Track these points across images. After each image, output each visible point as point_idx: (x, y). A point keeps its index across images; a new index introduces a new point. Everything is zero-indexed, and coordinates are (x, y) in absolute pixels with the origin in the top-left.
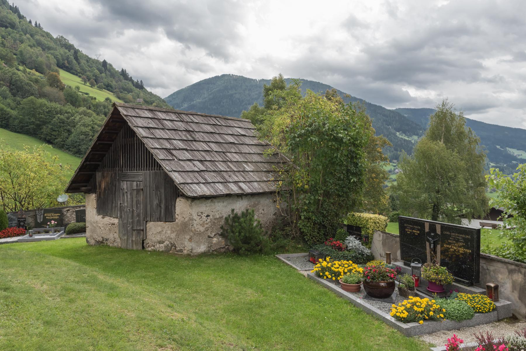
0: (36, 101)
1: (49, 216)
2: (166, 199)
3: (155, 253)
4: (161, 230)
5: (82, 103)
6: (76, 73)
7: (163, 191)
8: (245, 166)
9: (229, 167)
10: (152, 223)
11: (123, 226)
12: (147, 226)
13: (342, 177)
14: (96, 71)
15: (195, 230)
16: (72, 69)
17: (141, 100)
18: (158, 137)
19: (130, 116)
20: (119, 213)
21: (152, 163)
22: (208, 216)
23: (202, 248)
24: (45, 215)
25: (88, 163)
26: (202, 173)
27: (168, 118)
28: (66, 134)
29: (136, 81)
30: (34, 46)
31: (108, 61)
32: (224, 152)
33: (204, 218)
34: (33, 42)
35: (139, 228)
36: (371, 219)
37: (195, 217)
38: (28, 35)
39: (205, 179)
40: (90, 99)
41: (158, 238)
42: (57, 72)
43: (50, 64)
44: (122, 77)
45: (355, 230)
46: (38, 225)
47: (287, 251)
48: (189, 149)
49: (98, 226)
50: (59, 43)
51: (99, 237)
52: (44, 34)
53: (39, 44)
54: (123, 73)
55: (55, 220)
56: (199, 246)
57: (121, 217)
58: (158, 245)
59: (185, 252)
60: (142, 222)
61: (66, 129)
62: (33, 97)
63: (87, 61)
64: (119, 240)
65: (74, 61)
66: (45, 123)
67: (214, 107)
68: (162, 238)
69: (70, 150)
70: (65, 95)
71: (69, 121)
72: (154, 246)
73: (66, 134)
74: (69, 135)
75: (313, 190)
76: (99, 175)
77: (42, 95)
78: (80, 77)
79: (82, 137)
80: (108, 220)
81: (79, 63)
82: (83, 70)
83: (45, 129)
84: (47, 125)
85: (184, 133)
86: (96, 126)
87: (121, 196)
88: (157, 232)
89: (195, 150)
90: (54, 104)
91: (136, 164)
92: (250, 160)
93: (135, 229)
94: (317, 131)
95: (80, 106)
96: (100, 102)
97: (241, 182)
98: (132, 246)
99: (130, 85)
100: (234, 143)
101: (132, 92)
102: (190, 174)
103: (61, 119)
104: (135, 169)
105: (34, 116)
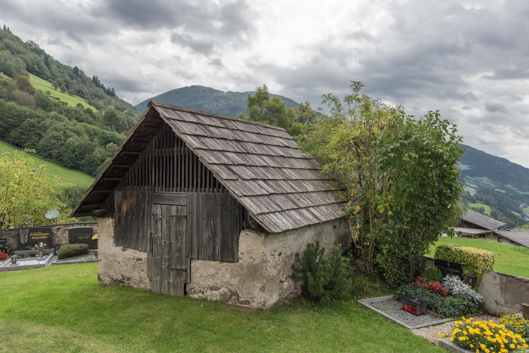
0: (5, 104)
1: (35, 236)
4: (215, 272)
5: (53, 108)
7: (219, 220)
10: (200, 261)
12: (192, 265)
13: (434, 202)
14: (68, 77)
15: (268, 275)
16: (42, 74)
17: (113, 107)
18: (212, 148)
19: (173, 119)
20: (148, 245)
22: (280, 254)
23: (274, 299)
24: (31, 235)
25: (106, 179)
26: (272, 197)
27: (213, 124)
28: (37, 138)
29: (107, 88)
31: (80, 68)
32: (279, 168)
35: (179, 267)
37: (269, 258)
40: (61, 104)
41: (211, 282)
42: (26, 75)
44: (93, 83)
45: (451, 265)
46: (21, 247)
48: (247, 164)
49: (116, 260)
50: (28, 47)
51: (116, 274)
52: (13, 38)
53: (8, 47)
54: (95, 81)
55: (43, 241)
56: (271, 296)
57: (152, 251)
58: (209, 292)
60: (184, 260)
61: (36, 133)
63: (58, 67)
64: (148, 281)
65: (45, 67)
66: (14, 126)
68: (216, 283)
69: (40, 154)
70: (35, 99)
71: (40, 125)
72: (203, 293)
73: (37, 138)
74: (40, 139)
76: (118, 195)
77: (11, 98)
78: (50, 82)
79: (53, 141)
80: (130, 253)
81: (50, 69)
82: (54, 75)
83: (14, 133)
84: (17, 129)
86: (68, 131)
87: (153, 223)
88: (208, 276)
89: (253, 166)
90: (24, 107)
91: (175, 182)
93: (173, 268)
95: (51, 110)
96: (71, 107)
97: (310, 207)
98: (169, 290)
102: (260, 198)
103: (31, 123)
104: (171, 189)
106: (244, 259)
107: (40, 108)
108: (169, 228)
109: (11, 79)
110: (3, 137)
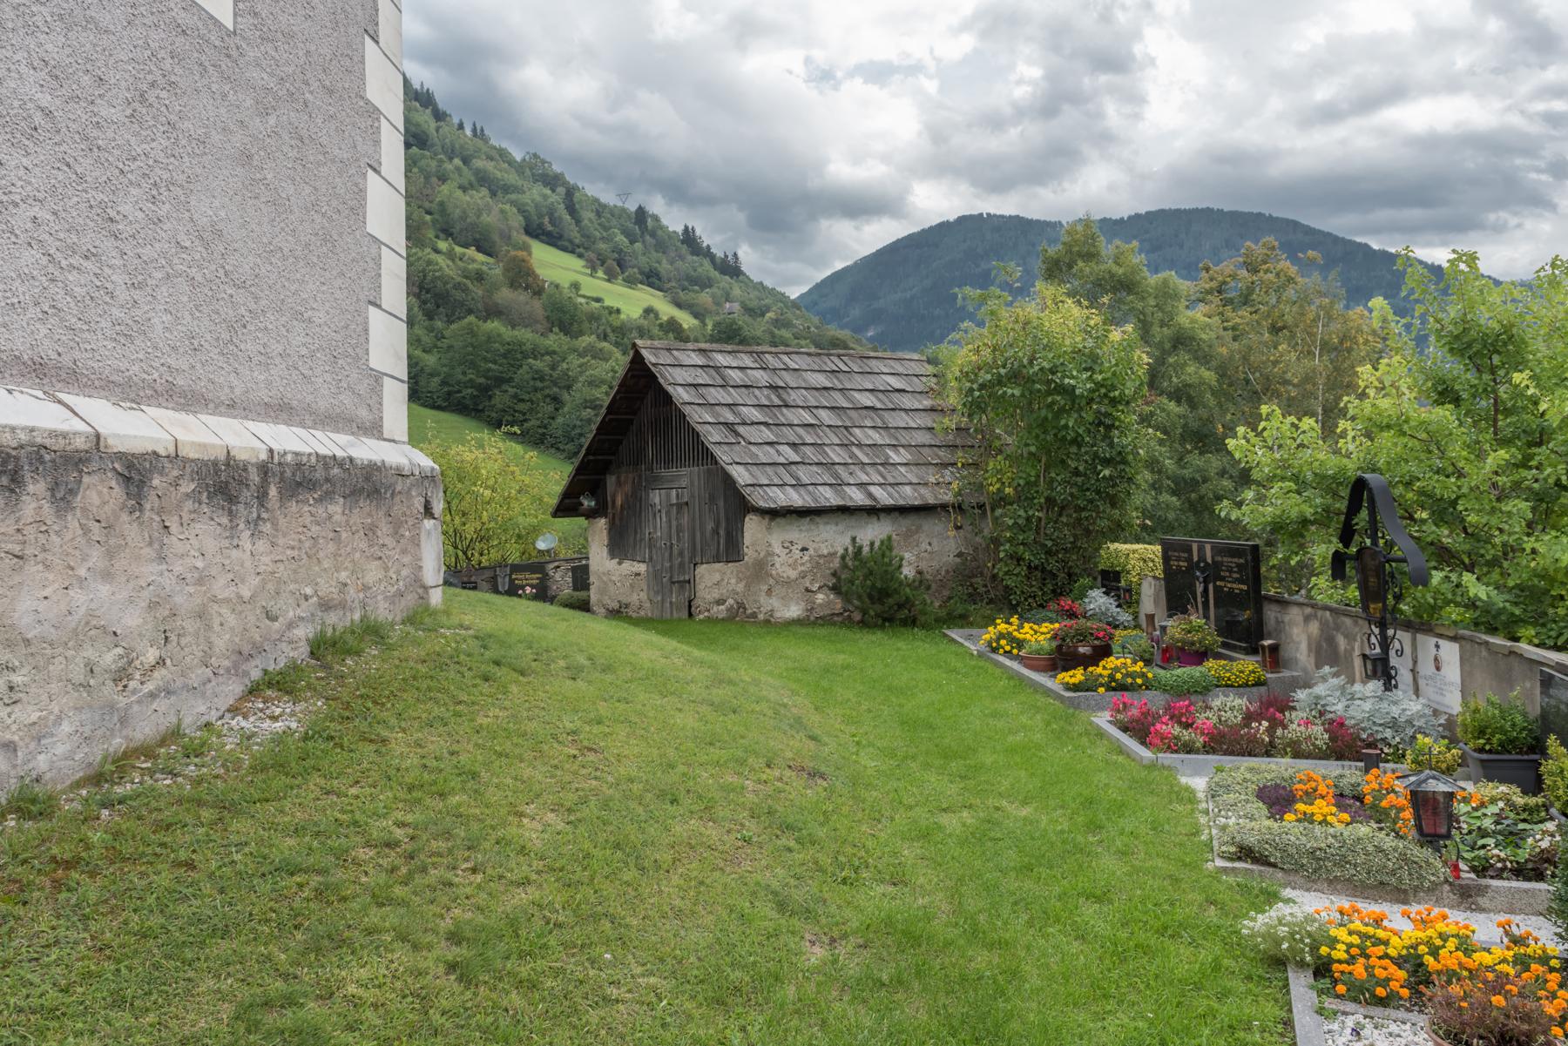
2: (727, 519)
3: (711, 621)
5: (586, 325)
6: (570, 249)
7: (721, 503)
8: (891, 453)
9: (852, 456)
11: (655, 576)
14: (621, 239)
16: (561, 237)
17: (736, 307)
21: (702, 454)
22: (804, 549)
23: (794, 611)
28: (550, 408)
29: (720, 254)
30: (472, 186)
32: (846, 428)
33: (797, 553)
34: (468, 175)
36: (1134, 552)
37: (777, 549)
38: (457, 161)
39: (798, 479)
41: (716, 595)
42: (526, 248)
43: (510, 229)
47: (971, 625)
52: (494, 153)
53: (483, 179)
55: (532, 586)
56: (787, 606)
57: (651, 559)
59: (761, 617)
62: (471, 318)
63: (599, 214)
64: (648, 605)
66: (500, 381)
67: (937, 312)
71: (555, 374)
73: (550, 408)
75: (1024, 496)
76: (611, 481)
77: (493, 312)
78: (580, 256)
80: (629, 567)
81: (578, 222)
83: (500, 399)
84: (504, 387)
85: (766, 392)
92: (903, 442)
94: (1015, 376)
95: (581, 333)
96: (630, 319)
99: (706, 268)
100: (872, 408)
101: (710, 286)
102: (768, 469)
103: (537, 372)
105: (473, 365)
106: (750, 554)
107: (556, 329)
108: (670, 521)
109: (491, 260)
110: (477, 411)
